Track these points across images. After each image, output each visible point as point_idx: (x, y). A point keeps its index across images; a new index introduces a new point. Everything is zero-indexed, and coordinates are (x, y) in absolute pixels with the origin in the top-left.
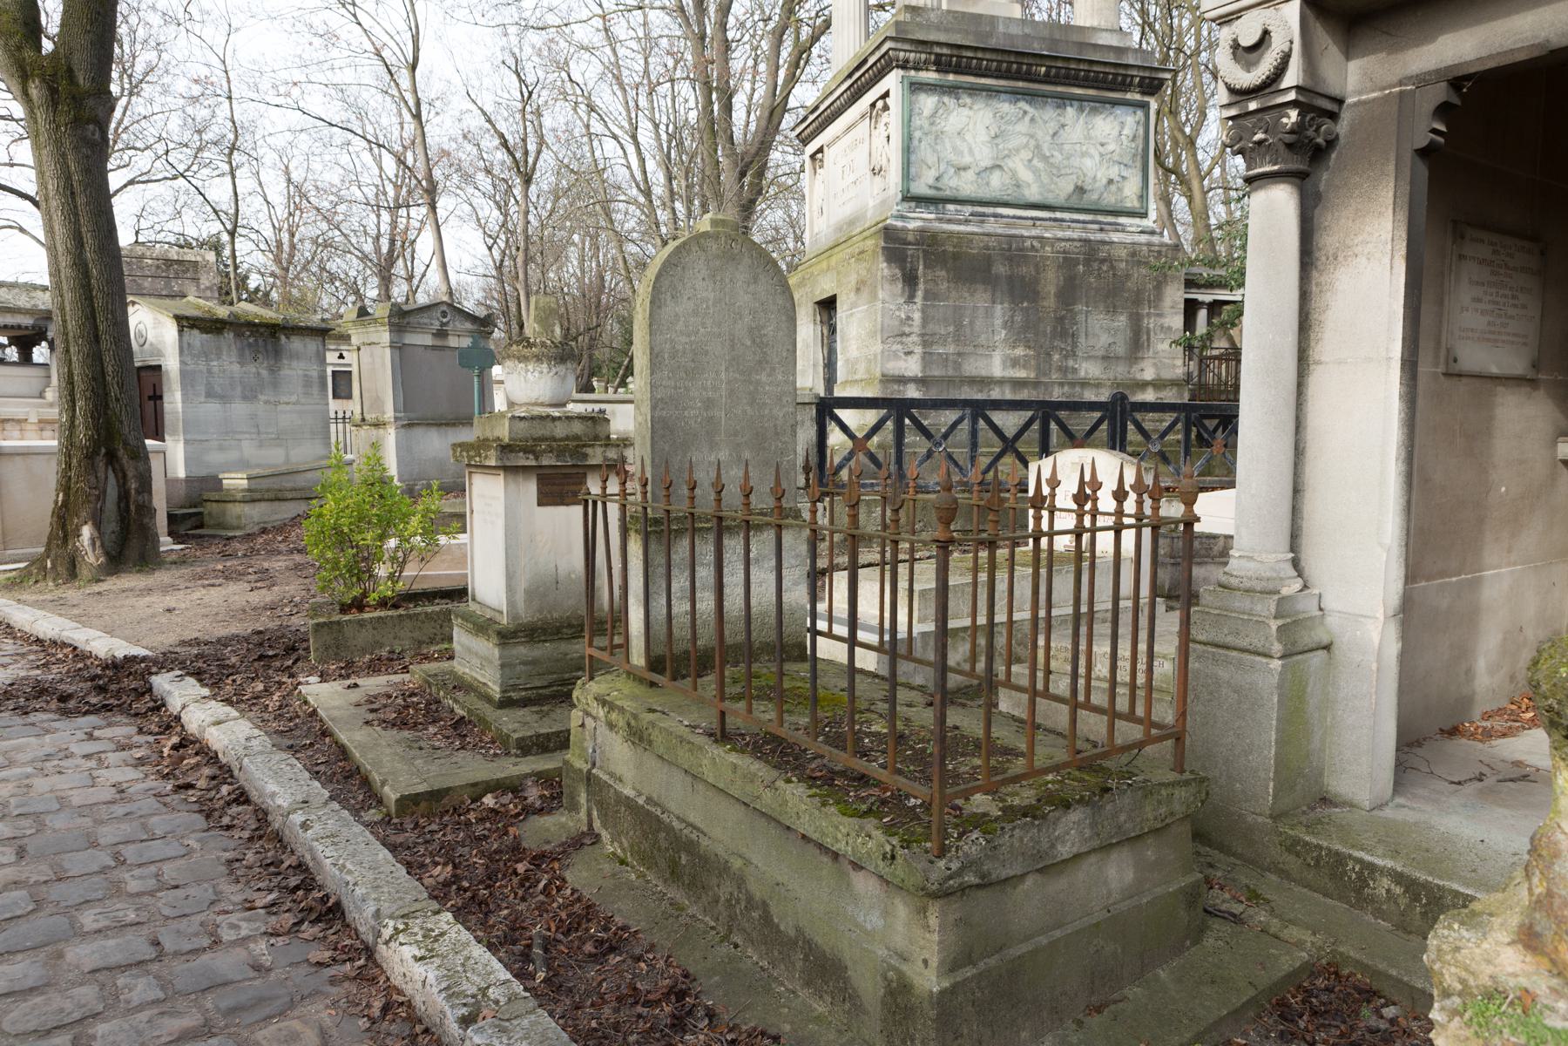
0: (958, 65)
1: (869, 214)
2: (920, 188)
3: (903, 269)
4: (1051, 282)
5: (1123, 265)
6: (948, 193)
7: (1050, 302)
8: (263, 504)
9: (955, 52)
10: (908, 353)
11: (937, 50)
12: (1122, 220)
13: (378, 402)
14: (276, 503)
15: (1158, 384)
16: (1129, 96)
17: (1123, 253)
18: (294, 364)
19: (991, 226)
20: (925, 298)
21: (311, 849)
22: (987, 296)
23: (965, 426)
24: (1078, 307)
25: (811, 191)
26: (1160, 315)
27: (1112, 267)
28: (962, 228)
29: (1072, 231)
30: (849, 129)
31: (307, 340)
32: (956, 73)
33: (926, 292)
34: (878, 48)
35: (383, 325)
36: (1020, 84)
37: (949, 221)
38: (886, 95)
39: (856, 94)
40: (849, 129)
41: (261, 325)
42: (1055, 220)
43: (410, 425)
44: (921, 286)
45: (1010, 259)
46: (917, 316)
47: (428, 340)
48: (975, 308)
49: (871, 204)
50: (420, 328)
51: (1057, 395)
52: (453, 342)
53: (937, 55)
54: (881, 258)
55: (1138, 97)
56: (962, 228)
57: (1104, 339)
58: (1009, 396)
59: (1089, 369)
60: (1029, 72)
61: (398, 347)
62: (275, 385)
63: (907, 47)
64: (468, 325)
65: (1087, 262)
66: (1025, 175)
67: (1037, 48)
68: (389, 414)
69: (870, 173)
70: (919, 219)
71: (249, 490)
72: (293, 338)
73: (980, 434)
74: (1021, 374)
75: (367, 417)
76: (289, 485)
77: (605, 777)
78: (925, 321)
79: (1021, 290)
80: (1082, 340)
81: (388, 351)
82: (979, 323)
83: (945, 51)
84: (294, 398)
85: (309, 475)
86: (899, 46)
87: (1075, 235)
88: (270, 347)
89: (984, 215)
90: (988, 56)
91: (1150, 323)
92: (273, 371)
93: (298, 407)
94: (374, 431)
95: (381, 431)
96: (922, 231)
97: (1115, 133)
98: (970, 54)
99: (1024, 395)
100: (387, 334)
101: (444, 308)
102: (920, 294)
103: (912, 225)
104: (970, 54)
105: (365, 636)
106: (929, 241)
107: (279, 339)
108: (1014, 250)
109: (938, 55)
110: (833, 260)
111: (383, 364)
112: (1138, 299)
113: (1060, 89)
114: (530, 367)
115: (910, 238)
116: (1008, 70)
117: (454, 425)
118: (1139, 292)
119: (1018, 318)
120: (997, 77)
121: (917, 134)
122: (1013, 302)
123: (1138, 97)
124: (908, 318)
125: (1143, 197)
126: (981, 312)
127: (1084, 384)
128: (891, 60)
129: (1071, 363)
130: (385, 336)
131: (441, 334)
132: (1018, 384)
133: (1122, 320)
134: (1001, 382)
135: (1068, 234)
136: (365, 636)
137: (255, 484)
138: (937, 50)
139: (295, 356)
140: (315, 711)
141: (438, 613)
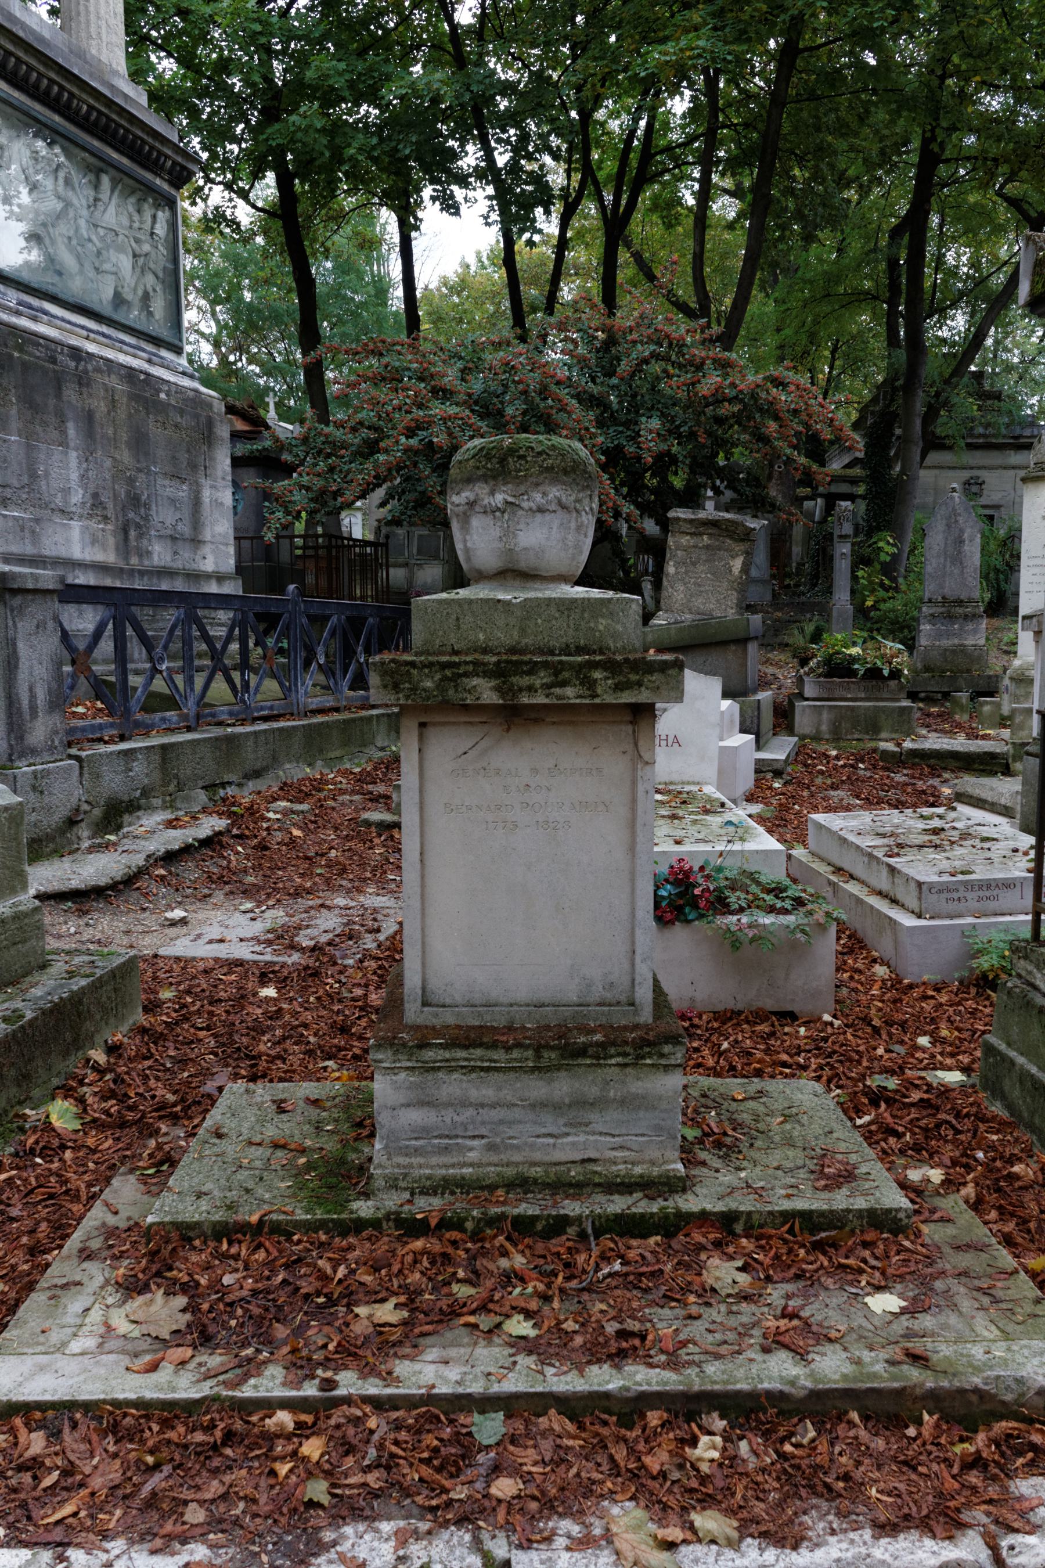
42: (104, 335)
56: (14, 320)
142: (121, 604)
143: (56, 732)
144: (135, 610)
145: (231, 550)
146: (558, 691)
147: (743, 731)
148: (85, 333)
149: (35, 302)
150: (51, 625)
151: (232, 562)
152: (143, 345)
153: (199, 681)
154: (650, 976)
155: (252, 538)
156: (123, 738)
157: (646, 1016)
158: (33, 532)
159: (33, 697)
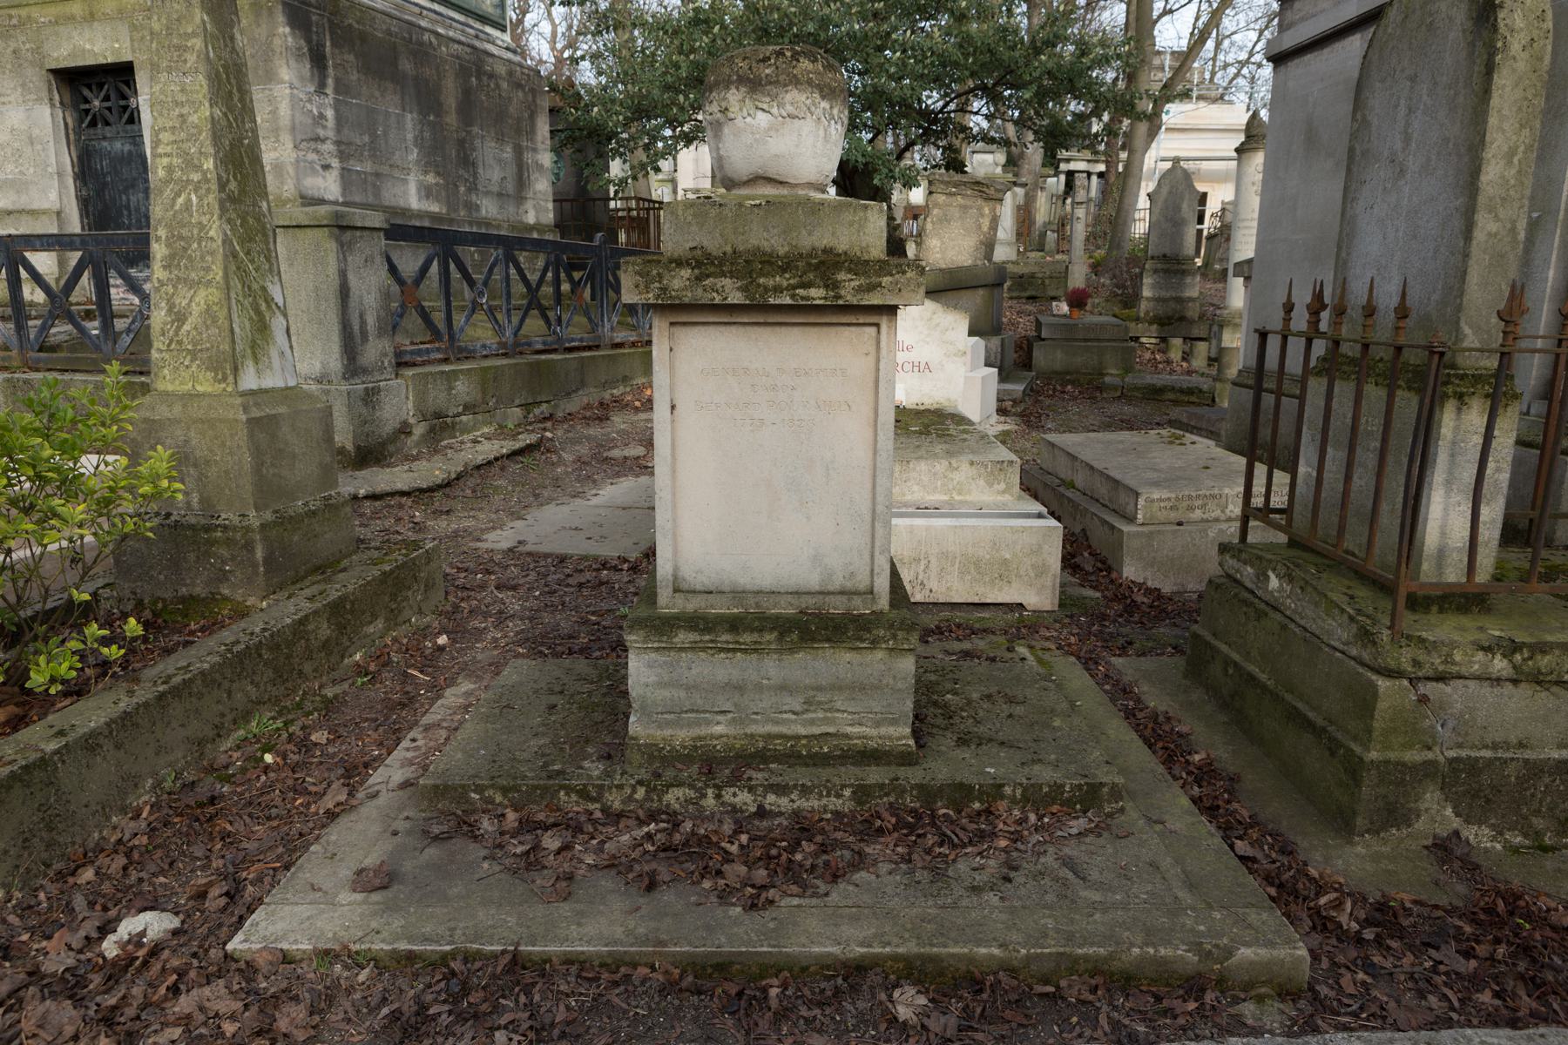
3: (309, 41)
5: (505, 85)
7: (452, 119)
10: (326, 167)
12: (488, 29)
20: (337, 91)
22: (397, 98)
24: (475, 130)
27: (498, 86)
33: (337, 81)
42: (435, 12)
44: (331, 71)
46: (330, 113)
54: (281, 18)
59: (489, 208)
73: (426, 282)
77: (1487, 754)
79: (426, 100)
80: (480, 171)
91: (528, 157)
102: (330, 81)
119: (427, 135)
122: (420, 113)
124: (322, 116)
126: (393, 119)
133: (508, 153)
135: (451, 34)
140: (516, 955)
142: (439, 239)
143: (386, 355)
144: (459, 249)
145: (550, 206)
146: (800, 292)
147: (987, 364)
148: (417, 10)
150: (379, 260)
151: (551, 215)
152: (471, 22)
153: (515, 320)
154: (887, 567)
155: (571, 201)
156: (446, 361)
157: (883, 603)
158: (374, 185)
159: (363, 323)
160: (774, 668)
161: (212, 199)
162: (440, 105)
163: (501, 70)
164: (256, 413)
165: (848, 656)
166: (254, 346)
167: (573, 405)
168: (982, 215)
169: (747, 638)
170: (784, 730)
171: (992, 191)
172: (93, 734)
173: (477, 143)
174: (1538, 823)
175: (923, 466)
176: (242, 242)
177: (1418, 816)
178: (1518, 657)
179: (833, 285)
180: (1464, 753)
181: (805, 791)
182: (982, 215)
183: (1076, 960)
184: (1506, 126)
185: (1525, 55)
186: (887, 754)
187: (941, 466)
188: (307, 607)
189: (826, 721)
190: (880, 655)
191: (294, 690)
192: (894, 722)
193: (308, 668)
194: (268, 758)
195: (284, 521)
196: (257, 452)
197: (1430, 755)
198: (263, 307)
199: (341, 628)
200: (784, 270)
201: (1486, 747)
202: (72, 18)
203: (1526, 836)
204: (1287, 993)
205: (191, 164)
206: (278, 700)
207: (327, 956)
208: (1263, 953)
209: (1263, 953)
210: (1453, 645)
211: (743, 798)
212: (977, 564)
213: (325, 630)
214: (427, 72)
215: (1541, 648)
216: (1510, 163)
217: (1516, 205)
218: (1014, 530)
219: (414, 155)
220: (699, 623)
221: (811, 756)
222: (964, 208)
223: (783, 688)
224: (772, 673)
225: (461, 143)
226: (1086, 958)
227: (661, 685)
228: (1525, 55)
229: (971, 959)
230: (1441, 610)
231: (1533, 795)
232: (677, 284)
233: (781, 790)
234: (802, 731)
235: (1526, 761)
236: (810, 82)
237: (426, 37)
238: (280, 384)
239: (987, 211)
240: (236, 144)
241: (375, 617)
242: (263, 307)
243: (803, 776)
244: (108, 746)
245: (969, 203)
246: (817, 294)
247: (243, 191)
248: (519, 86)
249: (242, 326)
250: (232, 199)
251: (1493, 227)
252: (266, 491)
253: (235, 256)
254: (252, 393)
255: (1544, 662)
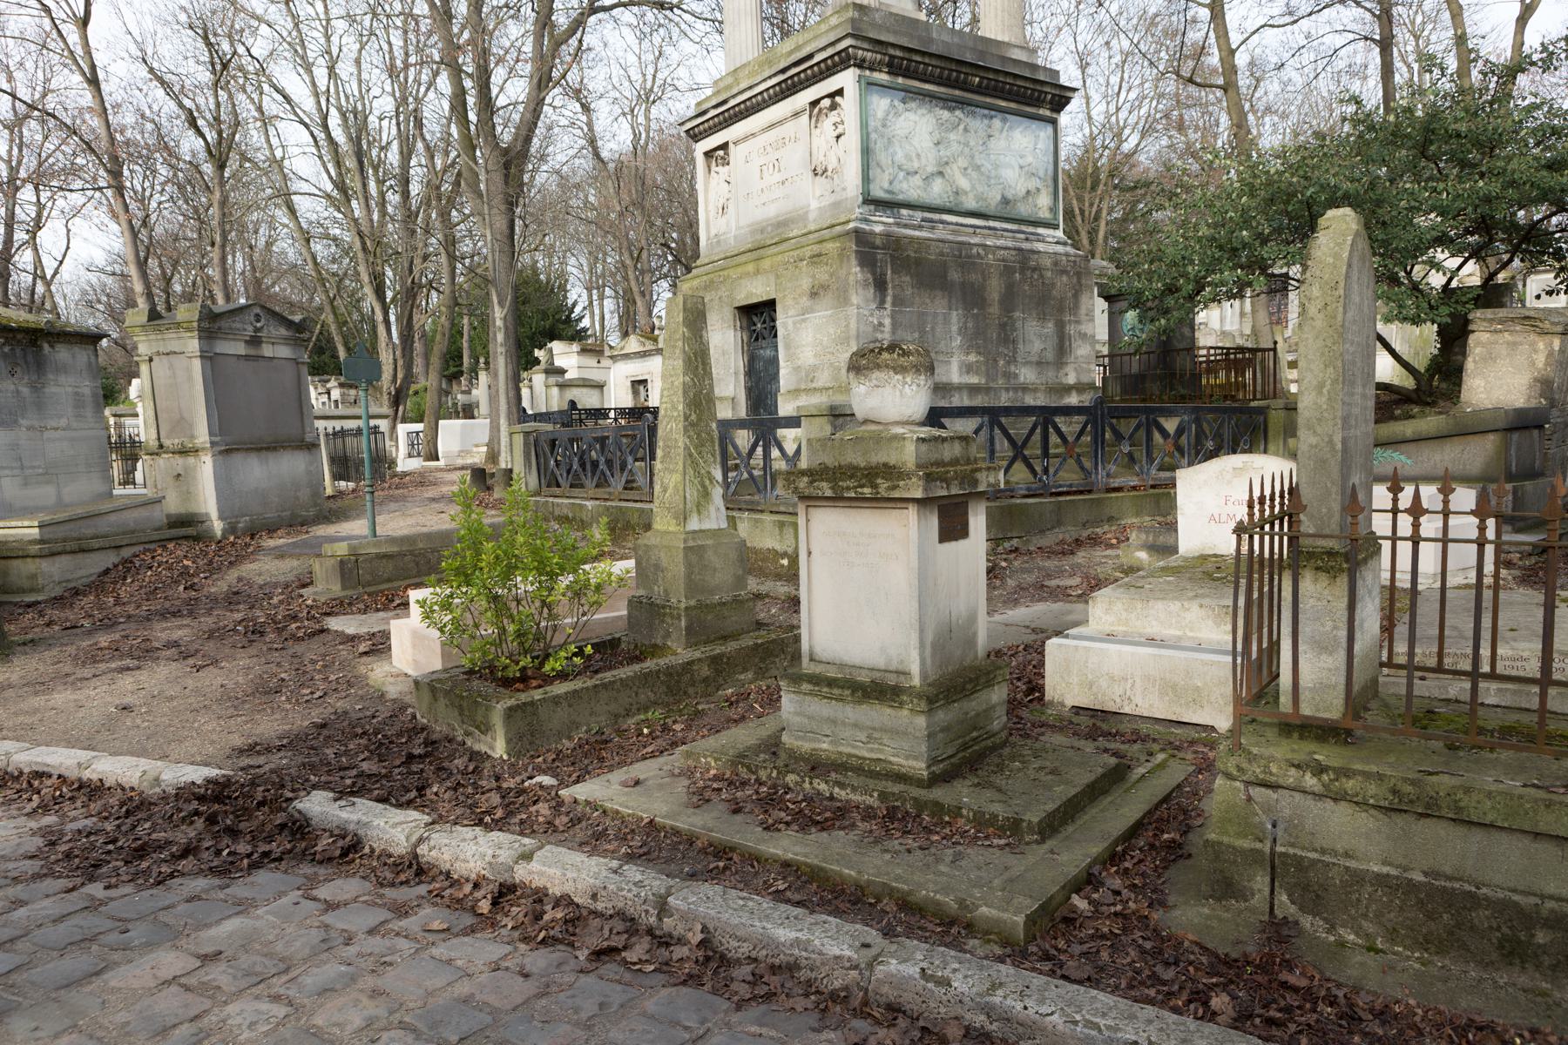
0: (908, 69)
1: (812, 216)
2: (878, 192)
3: (874, 274)
4: (995, 289)
5: (1049, 274)
6: (901, 197)
7: (995, 310)
8: (65, 559)
9: (907, 55)
11: (892, 51)
12: (1041, 231)
13: (182, 424)
14: (80, 556)
15: (1080, 388)
16: (1041, 112)
17: (1048, 262)
18: (62, 379)
19: (941, 233)
20: (894, 304)
21: (988, 1010)
22: (945, 302)
23: (984, 433)
24: (1017, 314)
25: (706, 190)
26: (1078, 322)
27: (1042, 276)
28: (917, 233)
29: (1002, 240)
30: (772, 126)
31: (76, 349)
32: (904, 76)
33: (895, 297)
34: (832, 44)
35: (189, 330)
36: (957, 92)
37: (906, 226)
38: (840, 92)
39: (787, 90)
40: (772, 126)
41: (20, 330)
42: (990, 228)
43: (228, 452)
44: (890, 291)
45: (962, 266)
46: (887, 321)
47: (240, 348)
48: (935, 315)
49: (814, 205)
50: (230, 335)
51: (1004, 400)
52: (267, 351)
53: (891, 57)
54: (854, 262)
55: (1048, 113)
56: (917, 233)
57: (1037, 346)
58: (966, 402)
59: (1027, 375)
60: (965, 82)
61: (208, 357)
62: (40, 406)
63: (865, 46)
64: (283, 331)
65: (1023, 270)
66: (964, 183)
67: (969, 58)
68: (202, 436)
69: (811, 174)
70: (880, 224)
71: (41, 541)
72: (59, 347)
74: (974, 380)
75: (167, 442)
76: (89, 532)
78: (895, 326)
79: (972, 297)
80: (1021, 346)
81: (197, 363)
82: (938, 329)
83: (898, 53)
84: (63, 422)
85: (113, 518)
86: (859, 44)
87: (1010, 244)
88: (30, 358)
89: (931, 221)
90: (934, 62)
91: (1071, 329)
92: (36, 388)
93: (69, 434)
94: (179, 460)
95: (191, 460)
96: (888, 235)
97: (1031, 146)
98: (919, 59)
99: (978, 401)
100: (195, 342)
101: (257, 310)
102: (889, 299)
103: (878, 229)
104: (919, 59)
105: (559, 717)
106: (893, 244)
107: (41, 348)
108: (963, 256)
109: (892, 57)
110: (766, 264)
111: (190, 379)
112: (1061, 310)
113: (988, 100)
114: (908, 380)
115: (878, 242)
116: (949, 78)
117: (275, 449)
118: (1062, 300)
119: (970, 325)
120: (938, 84)
121: (873, 136)
123: (1048, 113)
124: (881, 324)
125: (1053, 210)
126: (940, 318)
127: (1025, 389)
128: (849, 57)
129: (1013, 368)
130: (193, 345)
131: (255, 341)
132: (973, 390)
133: (1050, 327)
134: (959, 388)
135: (1000, 242)
136: (559, 717)
137: (50, 533)
138: (892, 51)
139: (62, 369)
141: (632, 679)
149: (936, 216)
152: (1024, 228)
160: (851, 712)
161: (681, 426)
162: (984, 300)
163: (1048, 262)
164: (691, 543)
165: (889, 711)
166: (698, 505)
167: (1049, 540)
168: (1536, 351)
169: (836, 691)
170: (856, 752)
171: (1547, 325)
172: (558, 696)
173: (1019, 324)
174: (1369, 927)
175: (1160, 605)
176: (696, 448)
177: (1253, 895)
178: (1325, 777)
179: (875, 486)
180: (1291, 851)
181: (854, 789)
182: (1536, 351)
183: (892, 889)
184: (1312, 366)
185: (1321, 316)
186: (911, 778)
187: (1175, 606)
188: (698, 655)
189: (881, 751)
190: (906, 712)
191: (679, 702)
192: (916, 758)
193: (691, 691)
194: (646, 731)
195: (701, 606)
196: (689, 566)
197: (1258, 845)
198: (707, 482)
199: (718, 672)
200: (851, 477)
201: (1316, 851)
202: (748, 274)
203: (1357, 934)
204: (1006, 942)
205: (674, 408)
206: (668, 705)
207: (588, 803)
208: (994, 912)
209: (994, 912)
210: (1271, 759)
211: (823, 787)
212: (1174, 687)
213: (705, 671)
214: (974, 277)
215: (1346, 773)
216: (1320, 393)
217: (1331, 423)
218: (1204, 663)
219: (958, 341)
220: (815, 680)
221: (871, 772)
222: (1513, 345)
223: (855, 725)
224: (850, 715)
225: (1003, 326)
226: (898, 890)
227: (797, 714)
228: (1321, 316)
229: (841, 875)
230: (1301, 738)
231: (1358, 900)
232: (802, 485)
233: (842, 786)
234: (867, 755)
235: (1347, 868)
236: (887, 366)
237: (974, 251)
238: (715, 526)
239: (1541, 346)
240: (698, 394)
241: (745, 670)
242: (707, 482)
243: (855, 780)
244: (564, 704)
245: (1518, 339)
246: (867, 491)
247: (699, 419)
248: (1064, 272)
249: (692, 494)
250: (692, 425)
251: (1313, 440)
252: (692, 587)
253: (691, 455)
254: (695, 532)
255: (1350, 785)
